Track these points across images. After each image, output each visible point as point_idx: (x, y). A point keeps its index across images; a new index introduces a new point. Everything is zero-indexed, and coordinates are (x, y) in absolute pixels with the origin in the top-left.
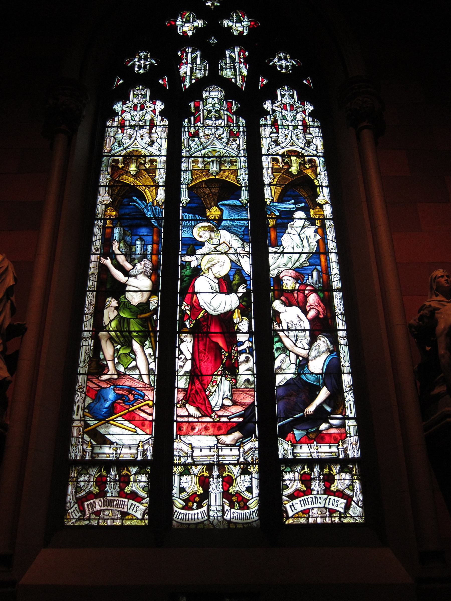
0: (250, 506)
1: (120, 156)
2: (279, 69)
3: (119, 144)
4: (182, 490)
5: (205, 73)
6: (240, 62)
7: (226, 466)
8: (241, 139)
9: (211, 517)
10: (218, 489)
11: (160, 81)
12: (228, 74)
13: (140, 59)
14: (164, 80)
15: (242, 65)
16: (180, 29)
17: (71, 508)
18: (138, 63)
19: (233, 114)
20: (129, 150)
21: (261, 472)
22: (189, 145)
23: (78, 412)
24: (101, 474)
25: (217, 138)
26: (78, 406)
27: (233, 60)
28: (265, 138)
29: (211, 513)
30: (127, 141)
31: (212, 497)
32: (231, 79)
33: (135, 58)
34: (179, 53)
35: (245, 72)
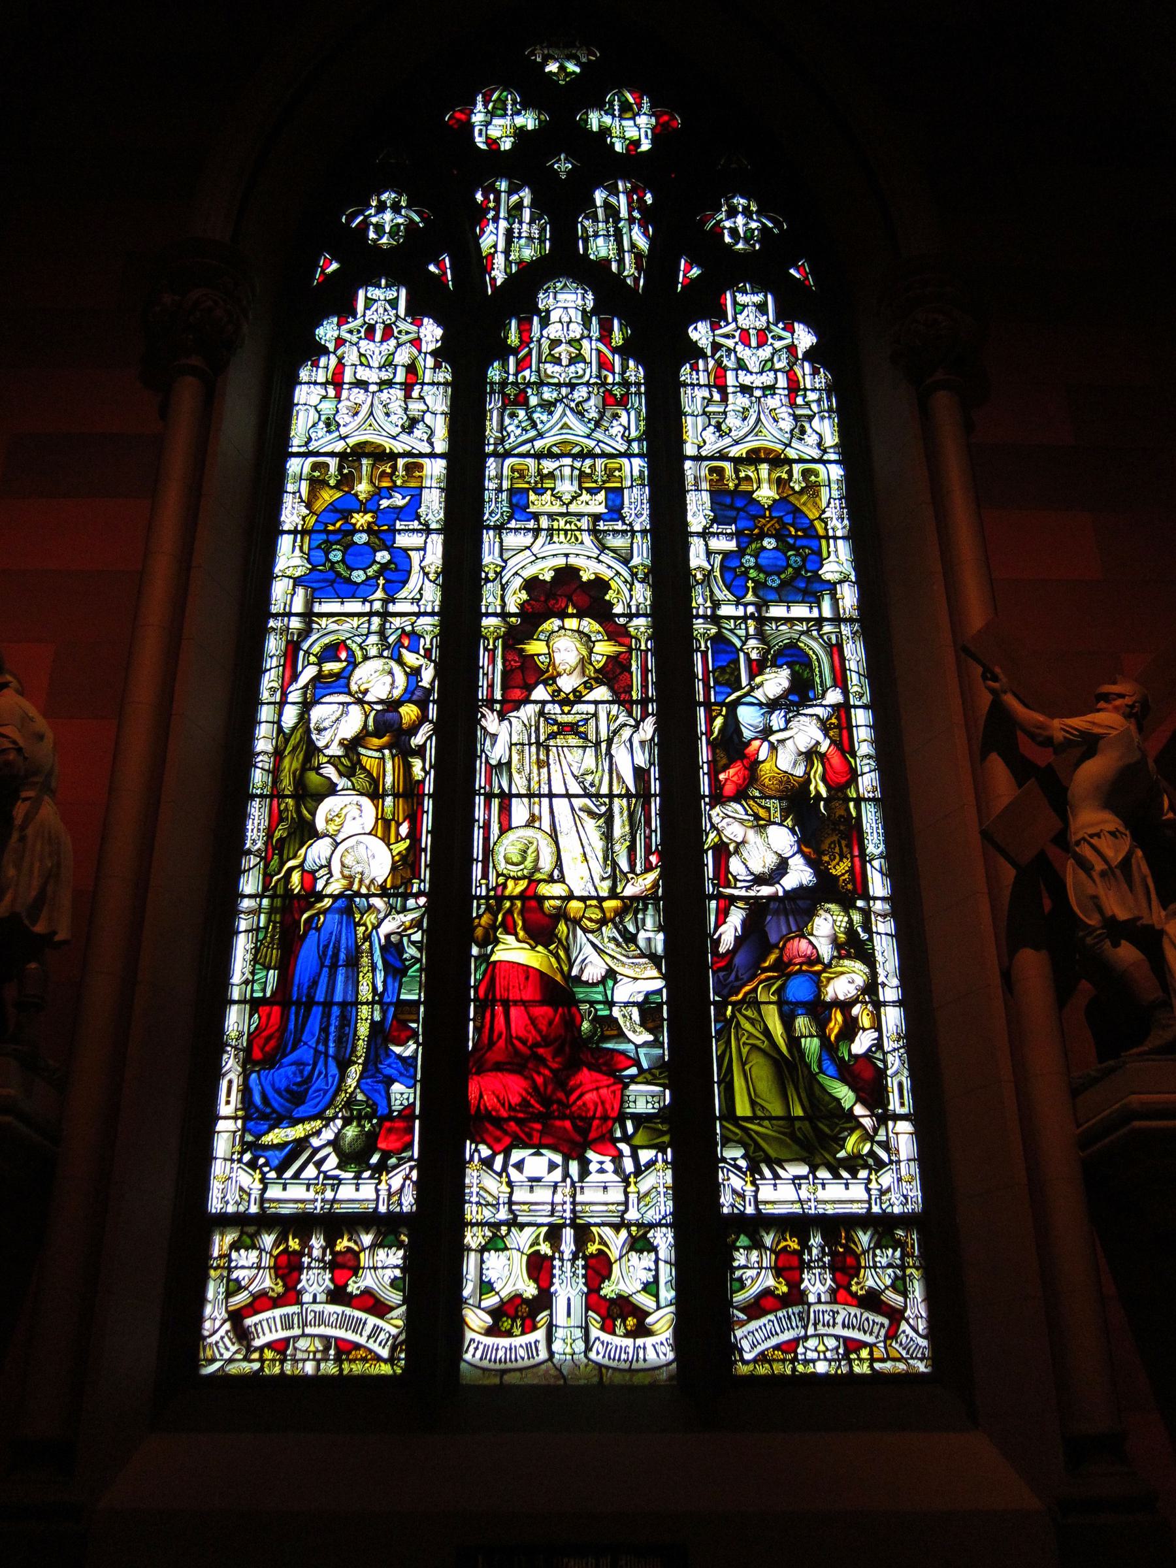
0: (655, 1328)
1: (332, 454)
2: (727, 239)
3: (328, 425)
4: (486, 1287)
5: (542, 248)
6: (631, 220)
7: (593, 1229)
8: (633, 413)
9: (557, 1356)
10: (321, 1282)
11: (432, 268)
12: (601, 248)
13: (381, 208)
14: (439, 265)
15: (636, 228)
16: (481, 130)
17: (215, 1332)
18: (728, 224)
19: (614, 351)
20: (352, 441)
21: (680, 1245)
22: (502, 428)
23: (229, 1094)
24: (288, 1246)
25: (571, 409)
26: (230, 1082)
27: (612, 212)
28: (692, 415)
29: (557, 1346)
30: (348, 419)
31: (560, 1305)
32: (609, 262)
33: (719, 210)
34: (479, 197)
35: (643, 244)
